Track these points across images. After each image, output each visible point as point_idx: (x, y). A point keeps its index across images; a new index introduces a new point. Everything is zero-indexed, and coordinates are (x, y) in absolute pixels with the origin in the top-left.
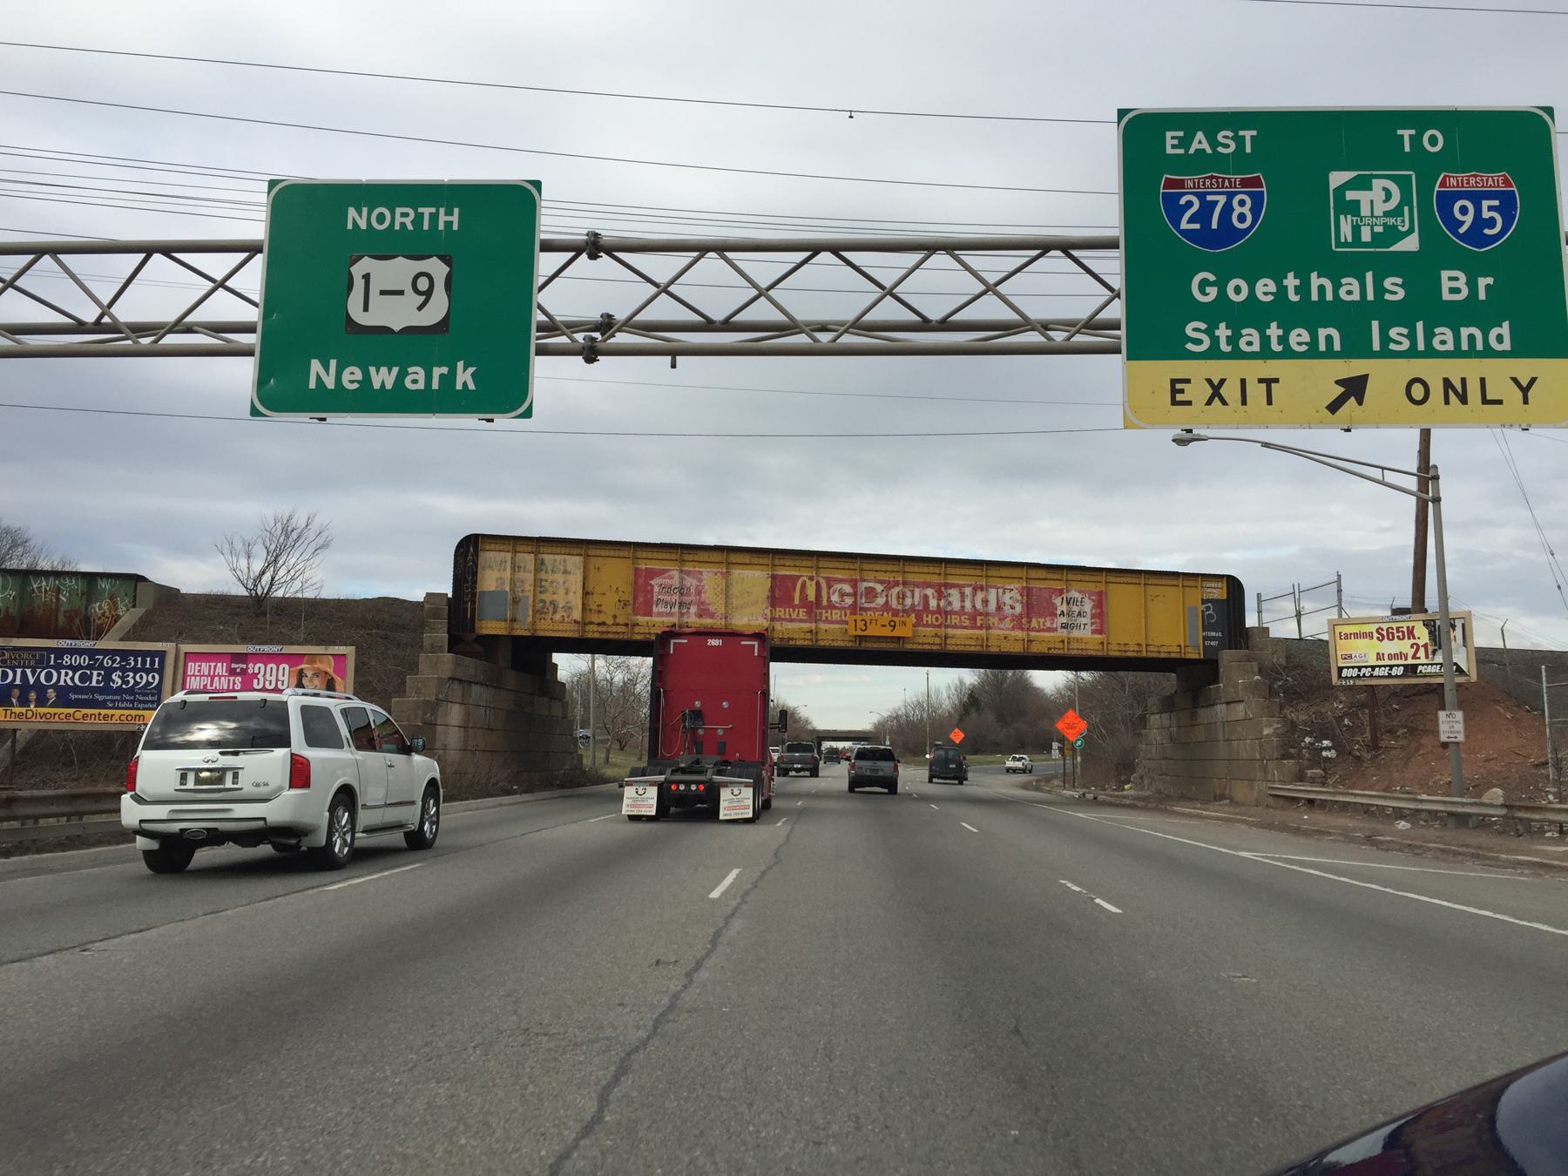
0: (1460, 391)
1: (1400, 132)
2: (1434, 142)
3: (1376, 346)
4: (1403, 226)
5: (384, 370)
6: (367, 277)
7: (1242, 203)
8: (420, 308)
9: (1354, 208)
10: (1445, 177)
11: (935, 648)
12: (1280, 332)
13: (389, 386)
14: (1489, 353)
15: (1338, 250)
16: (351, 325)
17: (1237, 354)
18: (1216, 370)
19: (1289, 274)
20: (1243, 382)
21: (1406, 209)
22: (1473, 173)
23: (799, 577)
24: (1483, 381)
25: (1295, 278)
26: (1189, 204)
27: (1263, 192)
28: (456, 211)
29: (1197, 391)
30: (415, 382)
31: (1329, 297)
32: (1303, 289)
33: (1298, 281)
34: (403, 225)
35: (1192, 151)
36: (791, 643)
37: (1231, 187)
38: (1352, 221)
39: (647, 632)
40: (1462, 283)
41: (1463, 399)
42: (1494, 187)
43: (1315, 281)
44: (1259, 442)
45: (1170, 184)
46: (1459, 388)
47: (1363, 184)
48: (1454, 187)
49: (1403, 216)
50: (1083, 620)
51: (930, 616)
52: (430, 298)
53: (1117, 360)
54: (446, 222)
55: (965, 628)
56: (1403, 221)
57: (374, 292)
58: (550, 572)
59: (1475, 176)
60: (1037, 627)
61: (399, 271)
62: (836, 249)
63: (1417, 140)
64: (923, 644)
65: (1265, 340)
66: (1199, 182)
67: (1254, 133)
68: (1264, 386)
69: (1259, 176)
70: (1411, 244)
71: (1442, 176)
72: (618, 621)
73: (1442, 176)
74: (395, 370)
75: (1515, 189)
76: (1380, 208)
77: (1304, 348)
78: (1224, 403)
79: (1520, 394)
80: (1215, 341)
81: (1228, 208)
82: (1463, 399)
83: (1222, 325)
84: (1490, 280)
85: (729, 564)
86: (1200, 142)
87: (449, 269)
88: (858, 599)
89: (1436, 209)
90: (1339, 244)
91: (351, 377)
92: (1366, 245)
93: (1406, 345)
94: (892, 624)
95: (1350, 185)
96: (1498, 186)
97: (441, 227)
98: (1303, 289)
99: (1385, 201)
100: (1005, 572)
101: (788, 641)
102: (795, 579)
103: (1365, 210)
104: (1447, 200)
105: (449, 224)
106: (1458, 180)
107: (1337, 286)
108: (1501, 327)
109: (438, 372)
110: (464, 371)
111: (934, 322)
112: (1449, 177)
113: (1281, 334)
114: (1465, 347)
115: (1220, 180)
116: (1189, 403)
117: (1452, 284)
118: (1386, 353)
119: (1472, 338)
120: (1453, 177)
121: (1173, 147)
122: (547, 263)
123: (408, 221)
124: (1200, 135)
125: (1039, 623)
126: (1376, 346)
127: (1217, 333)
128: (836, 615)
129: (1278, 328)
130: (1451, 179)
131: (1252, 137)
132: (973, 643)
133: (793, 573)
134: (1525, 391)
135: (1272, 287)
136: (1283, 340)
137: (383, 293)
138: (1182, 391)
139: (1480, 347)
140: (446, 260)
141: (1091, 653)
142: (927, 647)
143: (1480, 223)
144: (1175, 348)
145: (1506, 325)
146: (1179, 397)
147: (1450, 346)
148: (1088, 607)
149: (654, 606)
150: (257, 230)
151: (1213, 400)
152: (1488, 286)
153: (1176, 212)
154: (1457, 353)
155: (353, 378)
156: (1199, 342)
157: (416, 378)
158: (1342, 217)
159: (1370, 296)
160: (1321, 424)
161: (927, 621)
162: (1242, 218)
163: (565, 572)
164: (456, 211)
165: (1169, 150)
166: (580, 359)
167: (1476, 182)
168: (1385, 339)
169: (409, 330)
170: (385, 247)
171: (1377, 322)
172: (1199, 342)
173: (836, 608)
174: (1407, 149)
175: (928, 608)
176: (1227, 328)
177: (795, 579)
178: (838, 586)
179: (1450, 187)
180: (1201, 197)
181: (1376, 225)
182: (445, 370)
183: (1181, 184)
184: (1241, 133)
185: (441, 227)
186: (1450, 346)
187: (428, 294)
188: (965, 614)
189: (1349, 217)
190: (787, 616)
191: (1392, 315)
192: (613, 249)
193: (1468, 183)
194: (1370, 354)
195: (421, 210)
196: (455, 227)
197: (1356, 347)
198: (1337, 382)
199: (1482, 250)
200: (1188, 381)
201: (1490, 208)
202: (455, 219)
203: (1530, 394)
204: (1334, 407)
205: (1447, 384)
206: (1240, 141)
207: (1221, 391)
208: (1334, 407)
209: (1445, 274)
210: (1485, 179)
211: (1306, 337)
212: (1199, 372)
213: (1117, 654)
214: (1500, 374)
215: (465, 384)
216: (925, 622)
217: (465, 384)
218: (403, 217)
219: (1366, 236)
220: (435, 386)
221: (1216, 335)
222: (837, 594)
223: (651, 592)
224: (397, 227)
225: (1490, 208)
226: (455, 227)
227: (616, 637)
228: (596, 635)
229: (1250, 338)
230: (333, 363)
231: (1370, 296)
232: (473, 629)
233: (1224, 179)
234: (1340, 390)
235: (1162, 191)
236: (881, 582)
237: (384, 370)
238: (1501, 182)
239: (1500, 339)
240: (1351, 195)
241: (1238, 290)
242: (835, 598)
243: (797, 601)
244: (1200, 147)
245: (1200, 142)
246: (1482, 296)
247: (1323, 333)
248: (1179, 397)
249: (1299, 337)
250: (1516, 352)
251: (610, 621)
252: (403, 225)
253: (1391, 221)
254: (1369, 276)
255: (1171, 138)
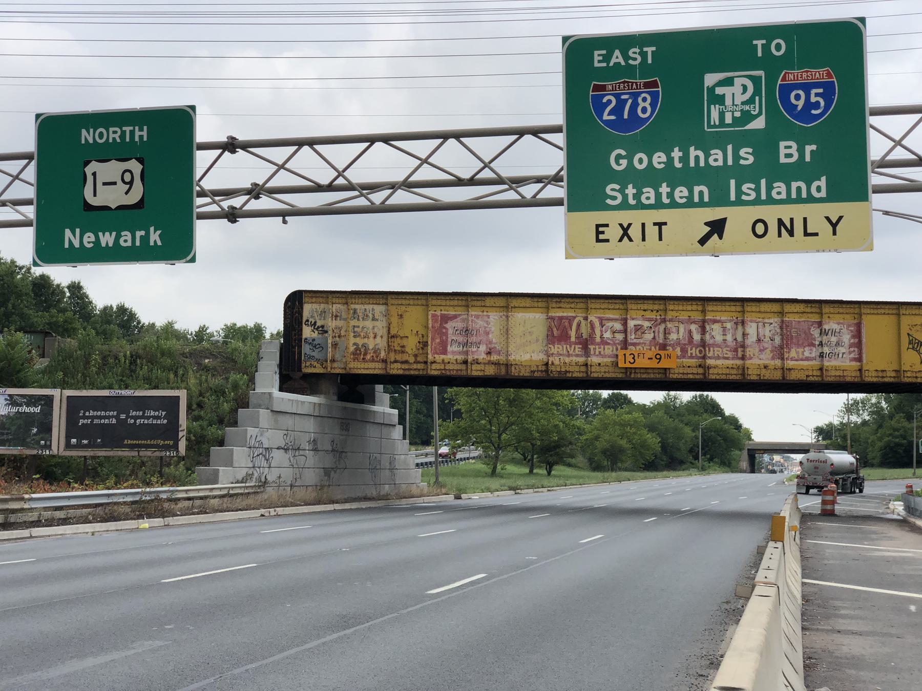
0: (783, 229)
1: (755, 42)
2: (779, 48)
3: (733, 197)
4: (754, 111)
5: (107, 234)
6: (94, 174)
7: (644, 100)
8: (127, 193)
9: (721, 100)
10: (785, 75)
11: (698, 377)
12: (669, 190)
13: (111, 245)
14: (811, 199)
15: (709, 130)
16: (88, 207)
17: (641, 206)
18: (625, 217)
19: (675, 149)
20: (643, 225)
21: (757, 98)
22: (805, 70)
23: (575, 317)
24: (805, 219)
25: (679, 151)
26: (610, 102)
27: (659, 91)
28: (145, 128)
29: (613, 232)
30: (126, 241)
31: (702, 164)
32: (685, 159)
33: (681, 153)
34: (114, 139)
35: (611, 64)
36: (569, 375)
37: (637, 89)
38: (719, 108)
39: (443, 368)
40: (794, 150)
41: (791, 233)
42: (820, 79)
43: (693, 153)
44: (881, 211)
45: (597, 88)
46: (788, 225)
47: (729, 82)
48: (791, 80)
49: (755, 104)
50: (842, 350)
51: (694, 349)
52: (132, 185)
53: (562, 210)
54: (140, 136)
55: (727, 358)
56: (755, 107)
57: (99, 185)
58: (361, 320)
59: (807, 72)
60: (796, 357)
61: (110, 170)
62: (387, 139)
63: (766, 48)
64: (687, 374)
65: (658, 195)
66: (616, 86)
67: (654, 49)
68: (657, 227)
69: (656, 80)
70: (759, 123)
71: (784, 72)
72: (418, 359)
73: (784, 72)
74: (114, 234)
75: (835, 80)
76: (740, 99)
77: (684, 200)
78: (630, 240)
79: (831, 228)
80: (625, 197)
81: (635, 105)
82: (791, 233)
83: (630, 186)
84: (814, 147)
85: (507, 308)
86: (617, 58)
87: (142, 166)
88: (629, 335)
89: (778, 97)
90: (709, 126)
91: (89, 238)
92: (729, 125)
93: (753, 195)
94: (658, 357)
95: (721, 83)
96: (823, 78)
97: (137, 139)
98: (685, 159)
99: (742, 94)
100: (764, 307)
101: (566, 374)
102: (570, 320)
103: (728, 101)
104: (786, 90)
105: (141, 137)
106: (794, 76)
107: (707, 156)
108: (820, 180)
109: (139, 234)
110: (155, 233)
111: (466, 181)
112: (788, 73)
113: (669, 191)
114: (794, 196)
115: (630, 84)
116: (607, 241)
117: (788, 151)
118: (739, 202)
119: (799, 189)
120: (791, 73)
121: (599, 61)
122: (202, 159)
123: (117, 136)
124: (617, 53)
125: (797, 353)
126: (733, 197)
127: (627, 191)
128: (609, 350)
129: (667, 187)
130: (790, 75)
131: (652, 51)
132: (735, 372)
133: (570, 314)
134: (834, 226)
135: (664, 158)
136: (670, 195)
137: (105, 184)
138: (603, 233)
139: (804, 195)
140: (140, 160)
141: (848, 379)
142: (691, 376)
143: (809, 105)
144: (598, 203)
145: (824, 179)
146: (601, 237)
147: (784, 196)
148: (847, 338)
149: (449, 346)
150: (30, 145)
151: (623, 238)
152: (812, 152)
153: (600, 107)
154: (788, 201)
155: (90, 240)
156: (614, 198)
157: (126, 239)
158: (712, 106)
159: (730, 162)
160: (694, 253)
161: (691, 354)
162: (644, 110)
163: (374, 319)
164: (145, 128)
165: (596, 65)
166: (225, 221)
167: (807, 76)
168: (739, 192)
169: (121, 208)
170: (105, 154)
171: (734, 180)
172: (614, 198)
173: (609, 344)
174: (760, 54)
175: (693, 342)
176: (633, 188)
177: (570, 320)
178: (610, 324)
179: (789, 81)
180: (617, 96)
181: (736, 111)
182: (143, 233)
183: (603, 88)
184: (645, 49)
185: (137, 139)
186: (784, 196)
187: (131, 183)
188: (727, 346)
189: (717, 106)
190: (565, 352)
191: (743, 174)
192: (246, 146)
193: (801, 77)
194: (726, 203)
195: (124, 128)
196: (145, 139)
197: (719, 198)
198: (706, 224)
199: (809, 126)
200: (607, 225)
201: (817, 95)
202: (145, 133)
203: (838, 228)
204: (703, 241)
205: (780, 222)
206: (644, 55)
207: (628, 232)
208: (703, 241)
209: (782, 144)
210: (813, 73)
211: (686, 193)
212: (614, 219)
213: (875, 380)
214: (817, 214)
215: (155, 241)
216: (689, 355)
217: (155, 241)
218: (114, 134)
219: (728, 119)
220: (138, 244)
221: (626, 193)
222: (609, 332)
223: (446, 334)
224: (111, 141)
225: (817, 95)
226: (145, 139)
227: (417, 373)
228: (401, 372)
229: (649, 195)
230: (78, 231)
231: (730, 162)
232: (300, 370)
233: (633, 83)
234: (708, 229)
235: (591, 93)
236: (649, 320)
237: (107, 234)
238: (825, 75)
239: (819, 189)
240: (719, 91)
241: (641, 161)
242: (607, 335)
243: (573, 339)
244: (617, 61)
245: (617, 57)
246: (808, 158)
247: (697, 189)
248: (601, 237)
249: (681, 193)
250: (830, 198)
251: (412, 359)
252: (114, 139)
253: (747, 108)
254: (730, 148)
255: (598, 55)
